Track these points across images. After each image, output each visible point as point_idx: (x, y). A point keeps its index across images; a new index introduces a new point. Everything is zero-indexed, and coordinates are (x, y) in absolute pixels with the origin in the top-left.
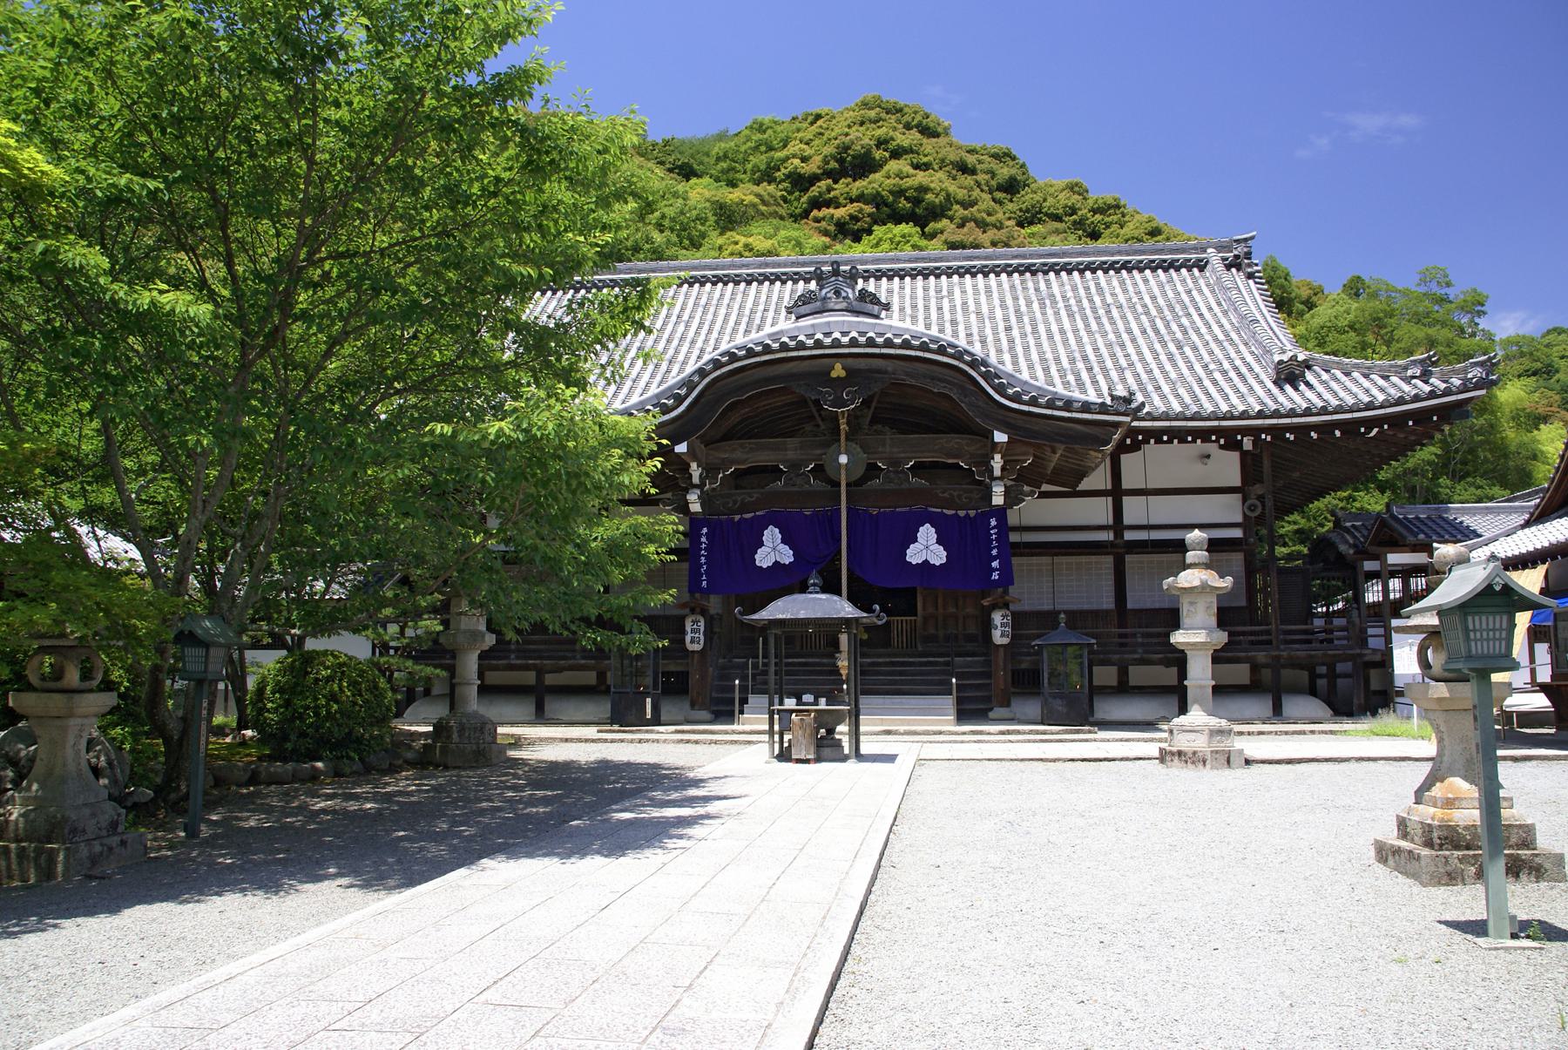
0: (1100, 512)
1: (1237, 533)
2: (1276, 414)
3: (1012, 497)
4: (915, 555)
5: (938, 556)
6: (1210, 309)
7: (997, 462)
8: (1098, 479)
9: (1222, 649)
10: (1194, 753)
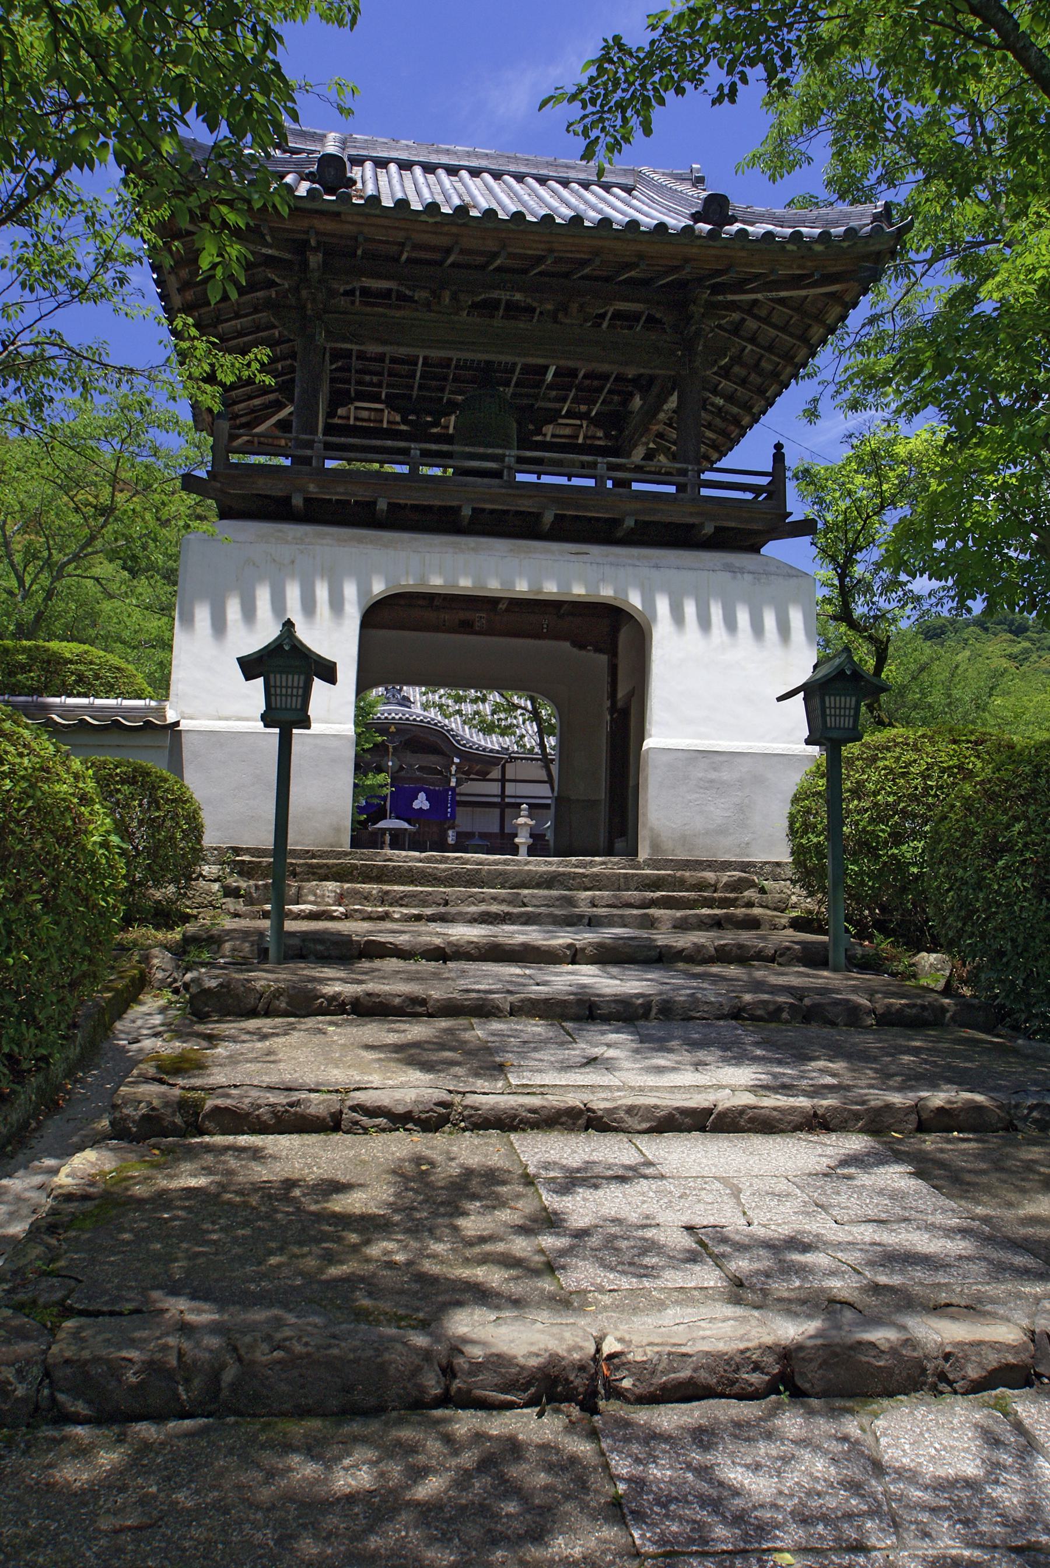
0: (494, 788)
3: (459, 783)
4: (416, 805)
5: (426, 806)
7: (454, 768)
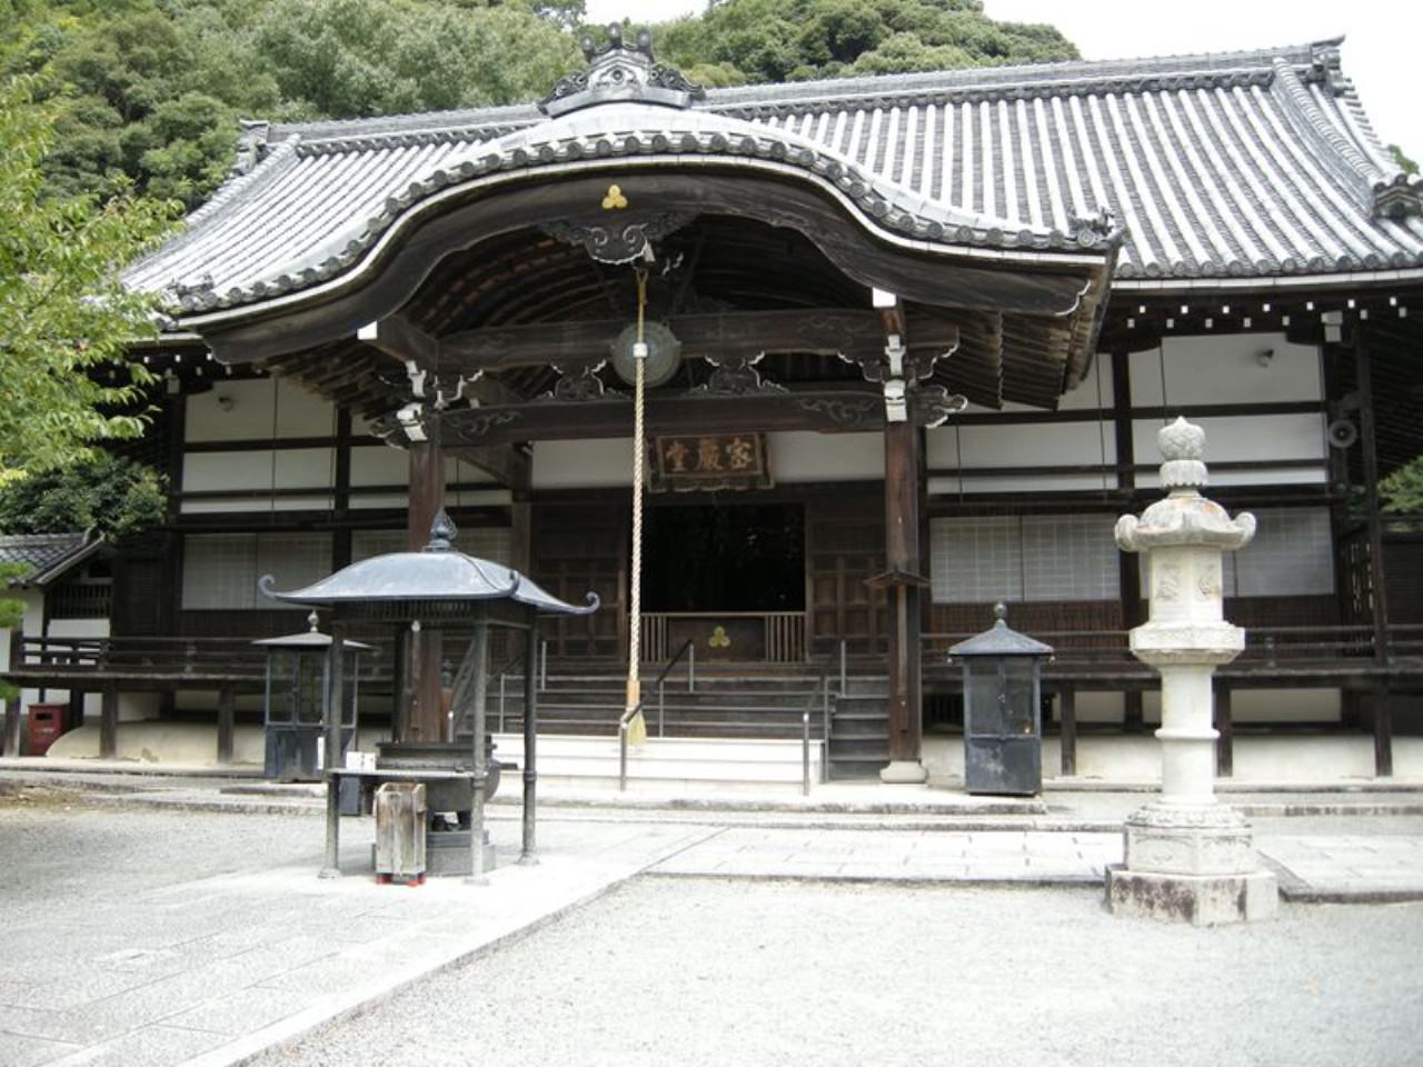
1: (1318, 477)
2: (1370, 265)
6: (1275, 136)
8: (1093, 390)
9: (1235, 665)
10: (1168, 886)
